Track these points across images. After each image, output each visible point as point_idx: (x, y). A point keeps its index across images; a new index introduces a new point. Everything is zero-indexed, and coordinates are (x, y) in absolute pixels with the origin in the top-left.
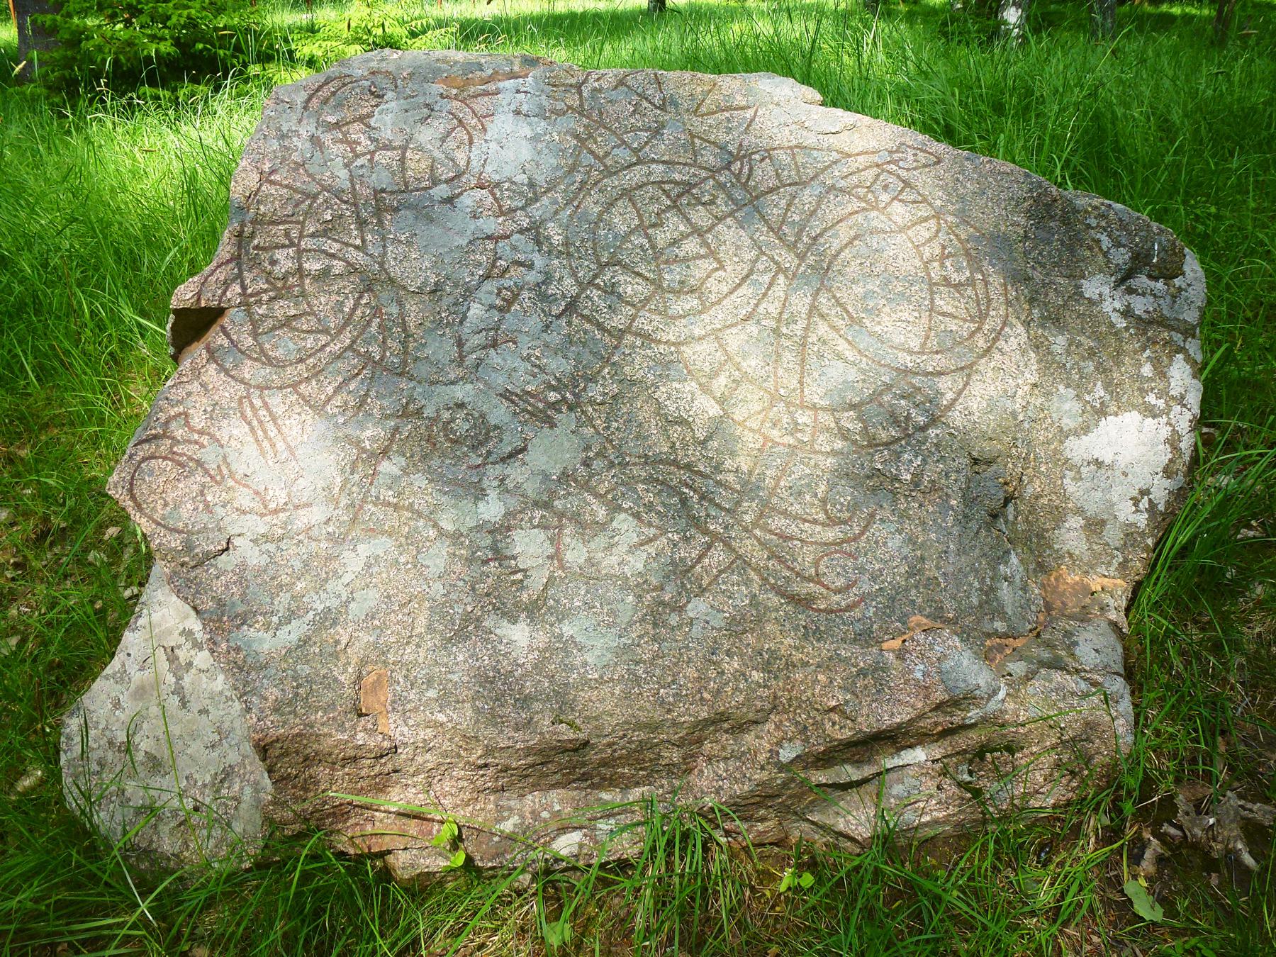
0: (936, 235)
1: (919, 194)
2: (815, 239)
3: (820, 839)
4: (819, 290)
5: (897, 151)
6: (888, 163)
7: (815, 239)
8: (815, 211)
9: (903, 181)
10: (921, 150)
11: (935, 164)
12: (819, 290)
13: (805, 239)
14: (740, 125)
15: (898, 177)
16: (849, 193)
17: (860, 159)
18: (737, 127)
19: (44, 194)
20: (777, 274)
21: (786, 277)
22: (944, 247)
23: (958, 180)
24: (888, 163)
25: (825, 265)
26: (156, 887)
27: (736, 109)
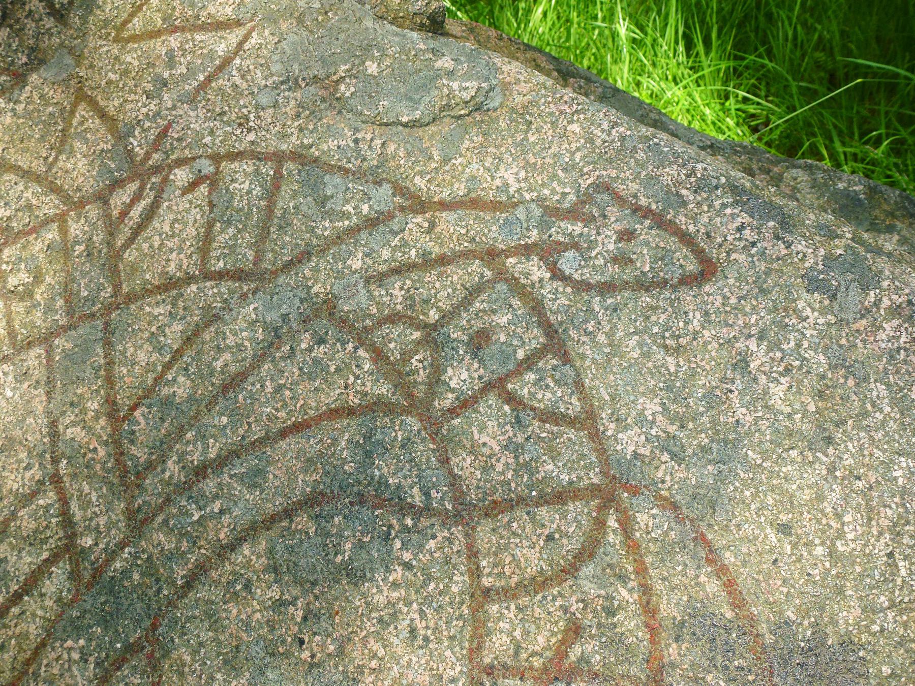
0: (570, 571)
1: (579, 386)
2: (201, 471)
3: (776, 15)
4: (131, 649)
5: (573, 214)
6: (527, 250)
7: (201, 471)
8: (242, 376)
9: (550, 330)
10: (661, 223)
11: (687, 281)
12: (131, 649)
13: (172, 467)
14: (191, 71)
15: (537, 307)
16: (362, 338)
17: (447, 222)
18: (184, 78)
19: (459, 180)
20: (54, 558)
21: (74, 576)
22: (575, 631)
23: (742, 363)
24: (527, 250)
25: (180, 573)
26: (810, 109)
27: (203, 28)
